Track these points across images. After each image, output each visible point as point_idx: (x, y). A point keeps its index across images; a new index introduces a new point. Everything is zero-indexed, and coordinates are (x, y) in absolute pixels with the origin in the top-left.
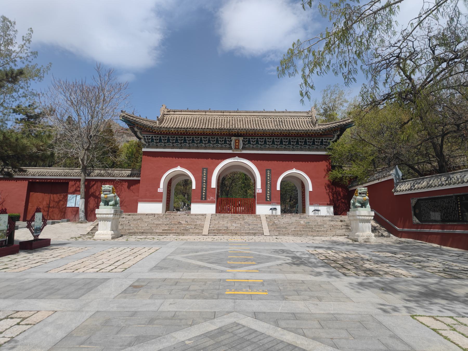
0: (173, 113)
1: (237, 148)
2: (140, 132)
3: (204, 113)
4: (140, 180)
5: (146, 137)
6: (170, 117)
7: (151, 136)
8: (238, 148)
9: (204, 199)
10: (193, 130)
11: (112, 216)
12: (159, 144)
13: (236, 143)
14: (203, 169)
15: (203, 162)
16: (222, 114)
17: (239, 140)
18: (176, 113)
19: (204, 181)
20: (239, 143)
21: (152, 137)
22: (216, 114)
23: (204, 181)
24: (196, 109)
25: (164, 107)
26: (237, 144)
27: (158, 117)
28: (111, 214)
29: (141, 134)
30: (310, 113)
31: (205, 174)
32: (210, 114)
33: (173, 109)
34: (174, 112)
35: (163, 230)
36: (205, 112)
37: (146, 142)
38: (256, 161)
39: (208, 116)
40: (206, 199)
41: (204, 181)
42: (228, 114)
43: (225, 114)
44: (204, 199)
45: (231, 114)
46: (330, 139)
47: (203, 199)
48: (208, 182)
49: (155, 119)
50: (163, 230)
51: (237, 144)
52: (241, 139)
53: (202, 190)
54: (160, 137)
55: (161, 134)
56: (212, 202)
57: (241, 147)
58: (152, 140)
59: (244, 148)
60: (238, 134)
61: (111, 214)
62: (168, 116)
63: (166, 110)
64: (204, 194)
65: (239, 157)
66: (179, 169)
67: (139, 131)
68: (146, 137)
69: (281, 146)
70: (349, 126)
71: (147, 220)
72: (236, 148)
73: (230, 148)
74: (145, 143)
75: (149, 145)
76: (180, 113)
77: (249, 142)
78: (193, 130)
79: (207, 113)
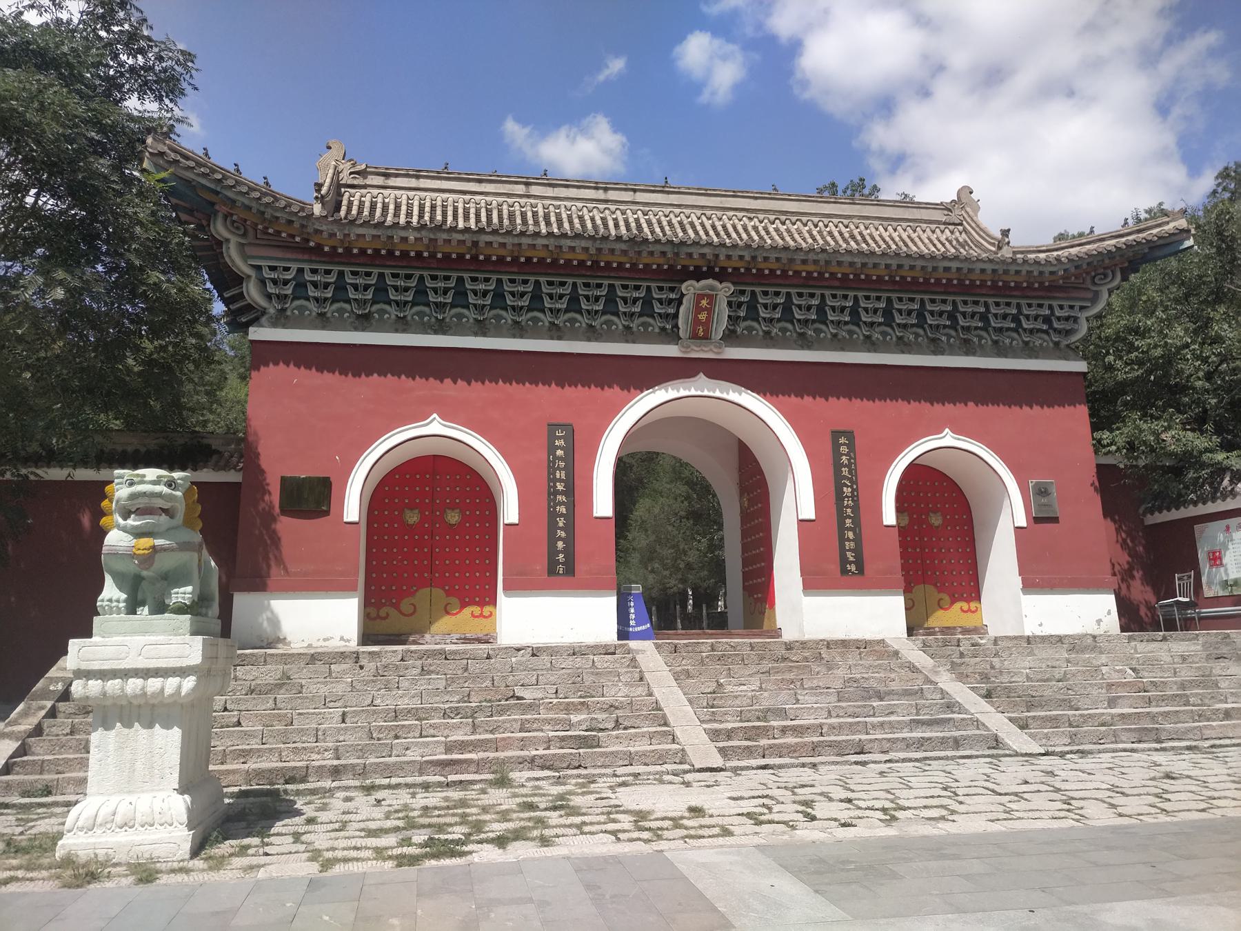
0: (379, 180)
1: (701, 334)
2: (241, 246)
3: (520, 189)
4: (236, 486)
5: (267, 274)
6: (367, 200)
7: (294, 266)
8: (707, 337)
9: (561, 569)
10: (509, 240)
11: (189, 683)
12: (330, 309)
13: (698, 309)
14: (553, 427)
15: (547, 400)
16: (600, 195)
17: (712, 299)
18: (392, 182)
19: (560, 487)
20: (710, 311)
21: (301, 271)
22: (573, 193)
23: (560, 486)
24: (485, 170)
25: (336, 152)
26: (703, 316)
27: (319, 186)
28: (182, 672)
29: (245, 257)
30: (957, 212)
31: (560, 453)
32: (550, 192)
33: (382, 166)
34: (387, 176)
35: (449, 748)
36: (527, 184)
37: (269, 297)
38: (786, 392)
39: (540, 204)
40: (570, 570)
41: (560, 487)
42: (627, 196)
43: (612, 195)
44: (561, 569)
45: (641, 197)
46: (1082, 308)
47: (560, 571)
48: (575, 489)
49: (309, 196)
50: (449, 748)
51: (703, 316)
52: (724, 291)
53: (552, 527)
54: (341, 274)
55: (348, 257)
56: (592, 586)
57: (721, 325)
58: (301, 286)
59: (731, 337)
60: (709, 264)
61: (182, 672)
62: (358, 194)
63: (346, 168)
64: (560, 545)
65: (712, 375)
66: (435, 426)
67: (234, 240)
68: (267, 274)
69: (888, 328)
70: (1167, 251)
71: (324, 690)
72: (694, 336)
73: (672, 336)
74: (262, 302)
75: (283, 310)
76: (413, 183)
77: (753, 314)
78: (509, 240)
79: (535, 190)
